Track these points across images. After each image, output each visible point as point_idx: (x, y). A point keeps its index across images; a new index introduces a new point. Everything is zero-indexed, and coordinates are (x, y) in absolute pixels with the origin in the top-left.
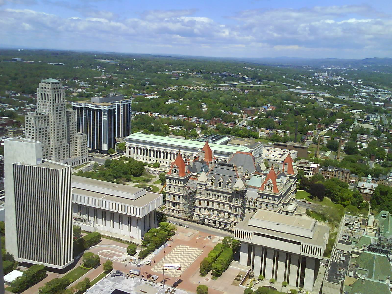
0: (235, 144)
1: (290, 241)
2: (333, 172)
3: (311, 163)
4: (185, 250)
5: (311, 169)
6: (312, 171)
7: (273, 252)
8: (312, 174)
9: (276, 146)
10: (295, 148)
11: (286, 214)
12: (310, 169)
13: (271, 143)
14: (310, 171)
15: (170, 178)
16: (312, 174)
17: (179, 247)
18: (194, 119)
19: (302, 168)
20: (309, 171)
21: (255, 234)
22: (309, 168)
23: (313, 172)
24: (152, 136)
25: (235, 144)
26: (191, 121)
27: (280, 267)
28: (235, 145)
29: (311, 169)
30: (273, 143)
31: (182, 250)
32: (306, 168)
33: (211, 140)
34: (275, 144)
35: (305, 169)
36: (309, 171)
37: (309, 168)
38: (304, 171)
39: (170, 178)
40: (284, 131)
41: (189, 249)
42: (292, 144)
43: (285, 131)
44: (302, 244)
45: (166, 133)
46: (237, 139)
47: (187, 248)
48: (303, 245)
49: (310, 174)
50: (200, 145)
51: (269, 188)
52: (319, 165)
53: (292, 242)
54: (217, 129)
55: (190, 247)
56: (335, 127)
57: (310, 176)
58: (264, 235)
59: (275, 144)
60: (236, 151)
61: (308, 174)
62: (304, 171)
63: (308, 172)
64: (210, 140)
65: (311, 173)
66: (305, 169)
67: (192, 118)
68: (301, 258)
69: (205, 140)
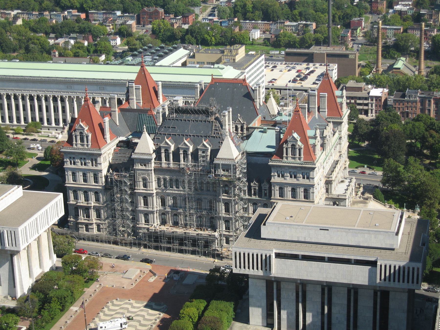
0: (203, 63)
1: (353, 262)
2: (416, 102)
3: (370, 86)
4: (127, 309)
5: (372, 100)
6: (374, 105)
7: (293, 286)
8: (374, 111)
9: (290, 57)
10: (332, 57)
11: (334, 204)
12: (370, 102)
13: (278, 52)
14: (370, 105)
15: (73, 156)
16: (374, 111)
17: (113, 305)
18: (102, 16)
19: (353, 101)
20: (367, 105)
21: (278, 255)
22: (366, 99)
23: (376, 106)
24: (17, 64)
25: (203, 63)
26: (95, 20)
27: (337, 318)
28: (205, 66)
29: (372, 100)
30: (283, 53)
31: (121, 311)
32: (360, 98)
33: (150, 60)
34: (287, 54)
35: (358, 101)
36: (367, 105)
37: (366, 99)
38: (358, 107)
39: (73, 156)
40: (302, 22)
41: (134, 307)
42: (324, 50)
43: (304, 22)
44: (379, 264)
45: (45, 54)
46: (205, 50)
47: (131, 304)
48: (381, 266)
49: (370, 111)
50: (127, 72)
51: (294, 153)
52: (386, 90)
53: (332, 260)
54: (154, 32)
55: (136, 303)
56: (406, 5)
57: (372, 116)
58: (324, 257)
59: (287, 54)
60: (210, 78)
61: (366, 113)
62: (358, 107)
63: (365, 108)
64: (148, 58)
65: (372, 110)
66: (358, 101)
67: (96, 15)
68: (379, 294)
69: (139, 60)
